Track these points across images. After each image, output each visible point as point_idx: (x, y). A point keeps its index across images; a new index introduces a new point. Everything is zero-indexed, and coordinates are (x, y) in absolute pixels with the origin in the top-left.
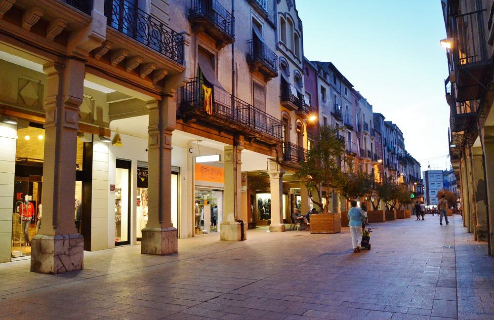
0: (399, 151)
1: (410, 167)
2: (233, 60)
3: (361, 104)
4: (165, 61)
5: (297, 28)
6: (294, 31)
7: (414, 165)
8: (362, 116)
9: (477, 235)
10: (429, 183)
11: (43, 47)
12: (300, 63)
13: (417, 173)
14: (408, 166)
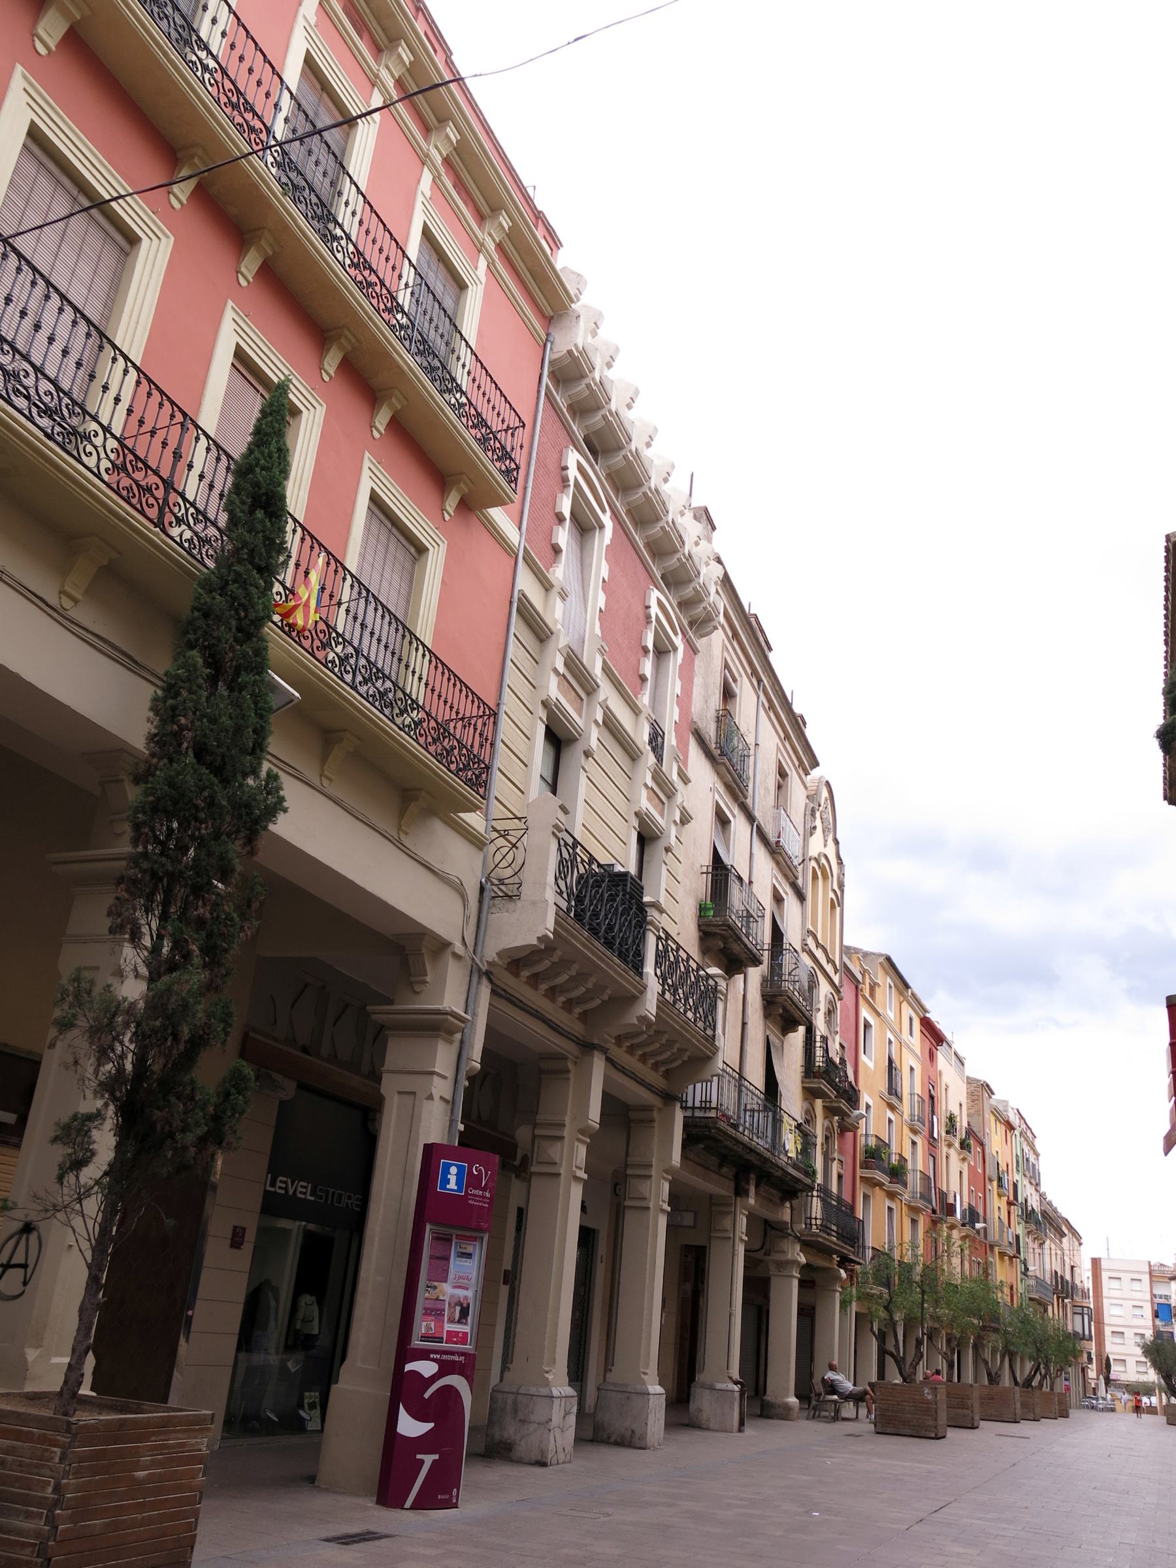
0: (1027, 1191)
1: (1053, 1246)
2: (744, 996)
3: (941, 1055)
4: (615, 971)
5: (836, 887)
6: (832, 895)
7: (1065, 1240)
8: (943, 1090)
9: (462, 1358)
10: (1105, 1301)
11: (505, 991)
12: (836, 971)
13: (1072, 1267)
14: (1048, 1242)
